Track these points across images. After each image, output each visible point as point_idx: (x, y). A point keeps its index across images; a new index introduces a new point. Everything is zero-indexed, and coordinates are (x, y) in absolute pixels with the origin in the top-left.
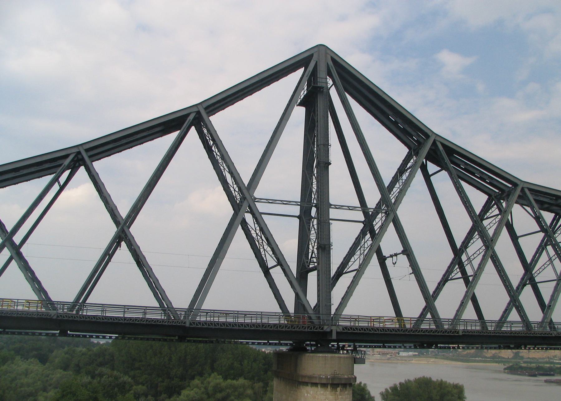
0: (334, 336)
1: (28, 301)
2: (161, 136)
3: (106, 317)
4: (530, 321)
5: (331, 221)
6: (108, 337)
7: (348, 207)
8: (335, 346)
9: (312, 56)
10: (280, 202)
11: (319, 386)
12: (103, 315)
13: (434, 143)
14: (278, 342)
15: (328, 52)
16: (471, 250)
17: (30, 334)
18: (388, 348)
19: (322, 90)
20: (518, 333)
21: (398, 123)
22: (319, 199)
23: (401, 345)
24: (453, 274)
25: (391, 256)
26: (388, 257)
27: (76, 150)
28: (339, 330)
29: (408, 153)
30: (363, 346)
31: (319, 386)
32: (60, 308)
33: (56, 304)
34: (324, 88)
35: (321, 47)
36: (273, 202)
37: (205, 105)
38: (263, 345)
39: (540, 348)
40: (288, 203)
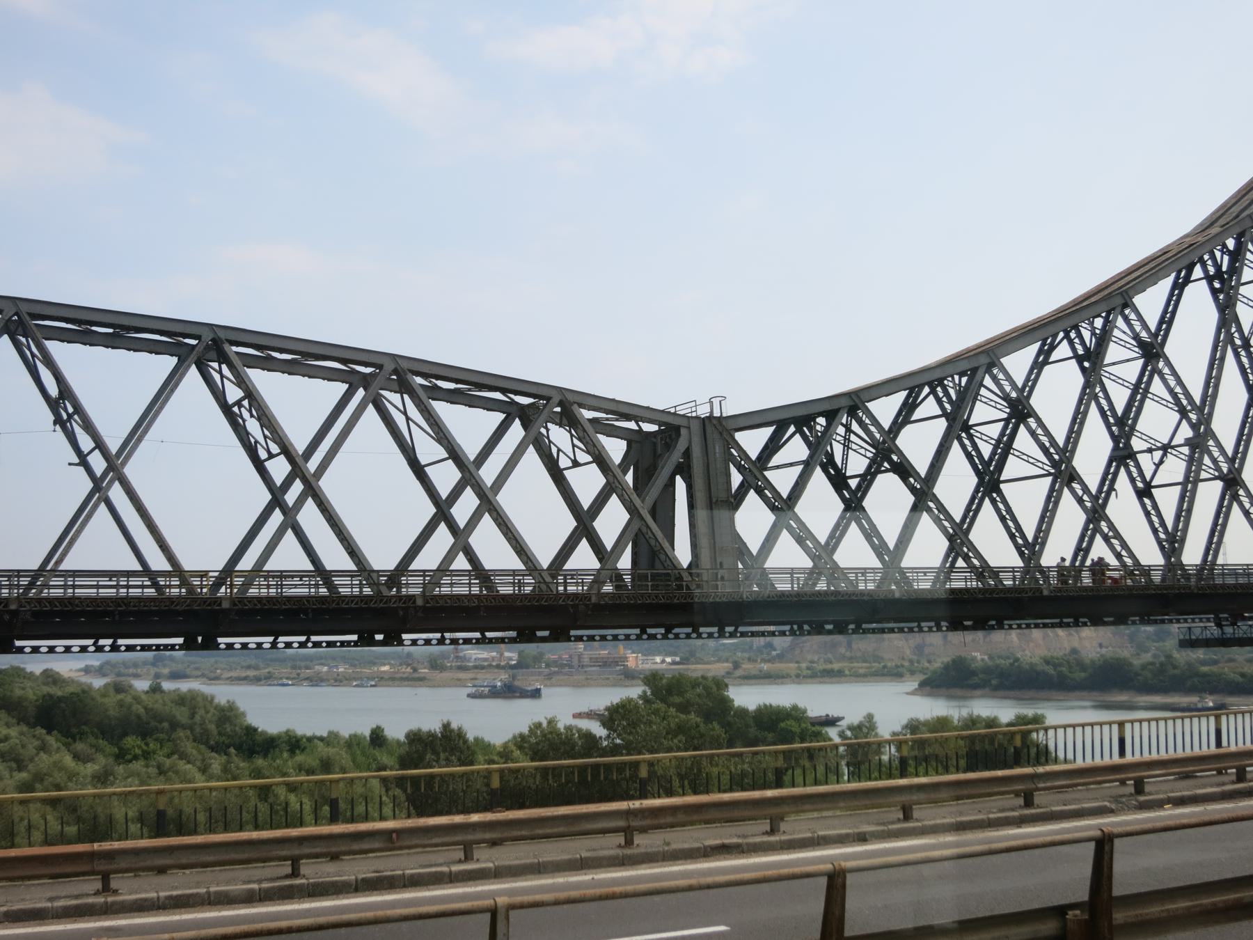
20: (386, 601)
22: (1216, 454)
32: (971, 579)
33: (492, 575)
39: (1024, 626)
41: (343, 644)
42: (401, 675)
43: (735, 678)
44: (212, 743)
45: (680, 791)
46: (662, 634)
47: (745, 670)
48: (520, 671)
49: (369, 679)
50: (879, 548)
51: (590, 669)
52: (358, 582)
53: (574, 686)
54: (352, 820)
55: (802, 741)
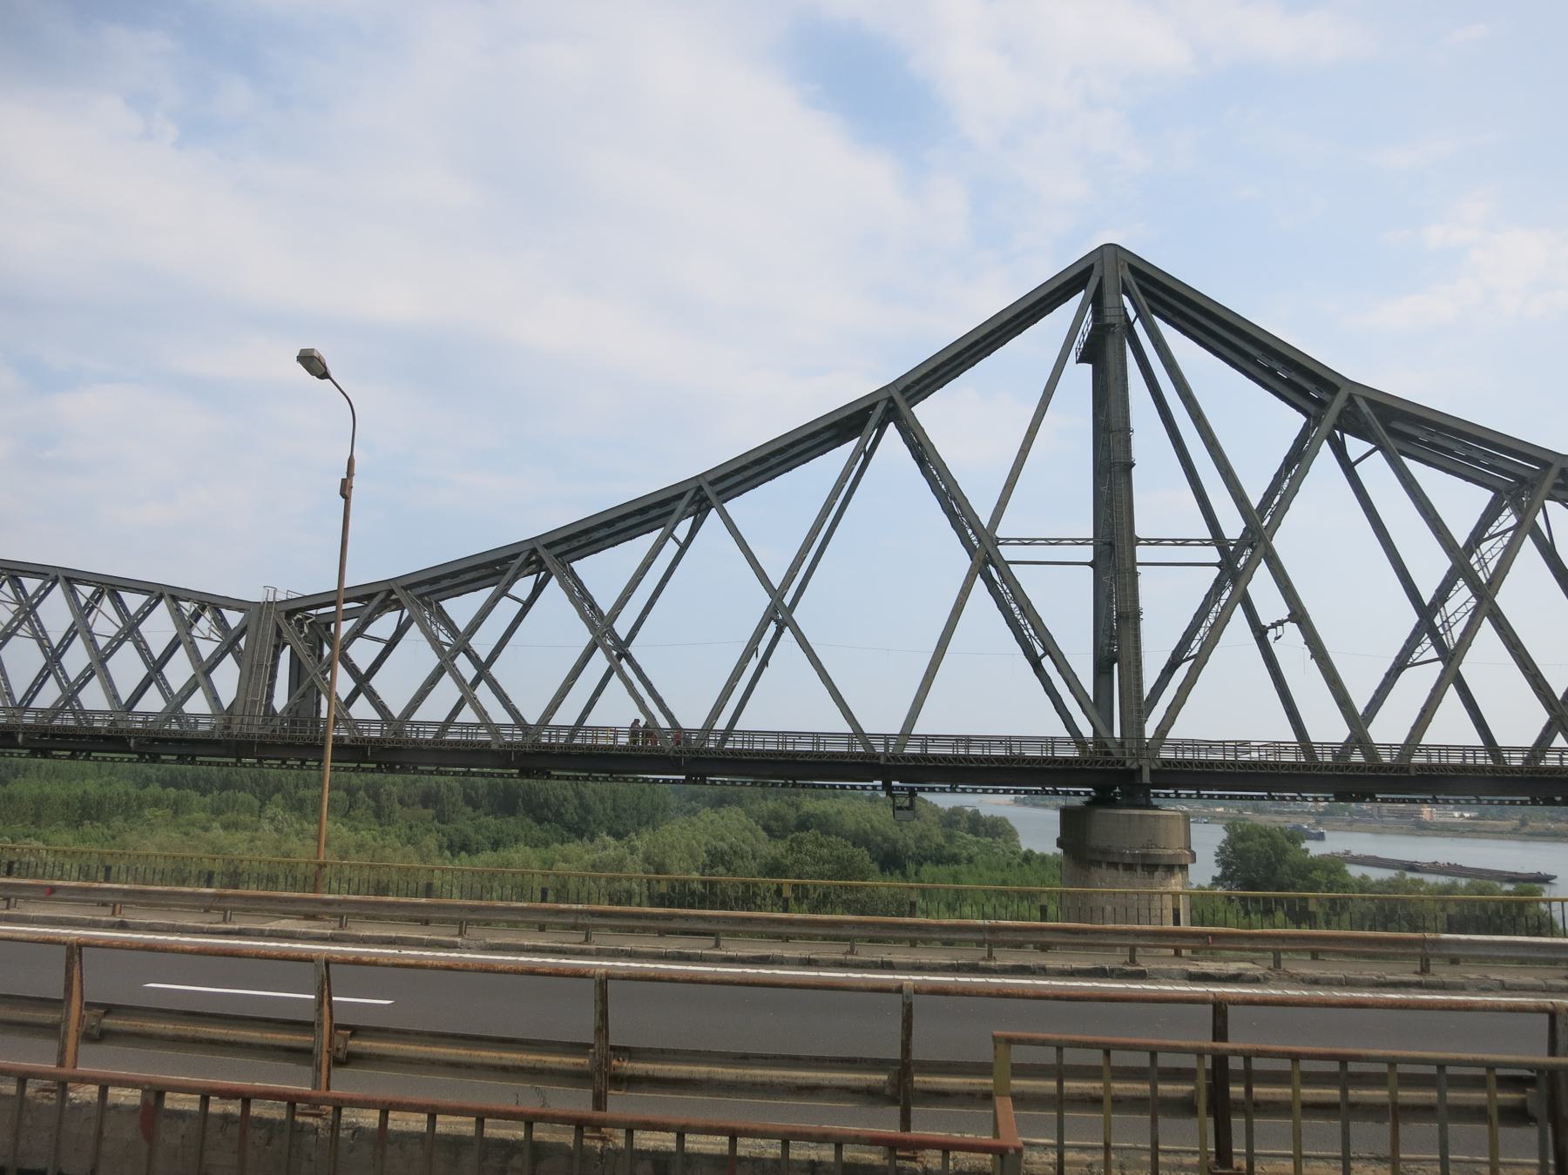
0: (1146, 779)
1: (1464, 748)
2: (839, 446)
3: (824, 754)
4: (1312, 741)
5: (1139, 569)
6: (991, 791)
7: (1046, 539)
8: (1171, 795)
9: (1091, 267)
10: (1198, 542)
11: (1139, 869)
12: (417, 736)
13: (1351, 399)
14: (1040, 788)
15: (1120, 254)
16: (1450, 606)
17: (859, 788)
18: (929, 791)
19: (1112, 329)
21: (1275, 371)
23: (1296, 795)
24: (1415, 656)
25: (1274, 626)
26: (1270, 628)
27: (694, 484)
28: (1154, 767)
29: (1305, 424)
30: (1012, 792)
31: (1139, 869)
34: (1117, 326)
35: (1106, 249)
36: (1032, 542)
37: (901, 386)
38: (1003, 793)
40: (1076, 542)
41: (675, 781)
42: (1228, 815)
43: (1520, 834)
44: (910, 854)
45: (936, 916)
46: (298, 766)
47: (1532, 827)
48: (1326, 817)
49: (1203, 817)
50: (113, 695)
51: (1386, 819)
52: (547, 733)
53: (1373, 833)
54: (1213, 925)
55: (1330, 890)
